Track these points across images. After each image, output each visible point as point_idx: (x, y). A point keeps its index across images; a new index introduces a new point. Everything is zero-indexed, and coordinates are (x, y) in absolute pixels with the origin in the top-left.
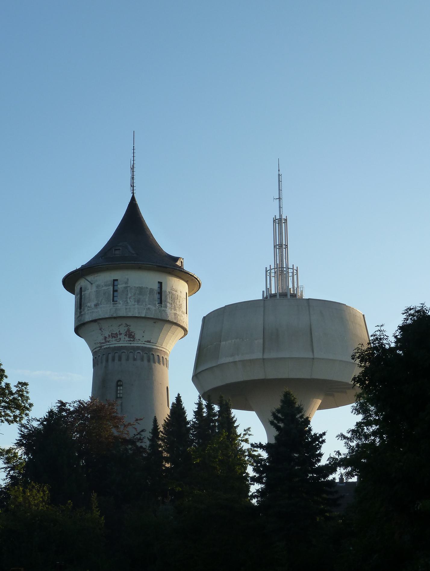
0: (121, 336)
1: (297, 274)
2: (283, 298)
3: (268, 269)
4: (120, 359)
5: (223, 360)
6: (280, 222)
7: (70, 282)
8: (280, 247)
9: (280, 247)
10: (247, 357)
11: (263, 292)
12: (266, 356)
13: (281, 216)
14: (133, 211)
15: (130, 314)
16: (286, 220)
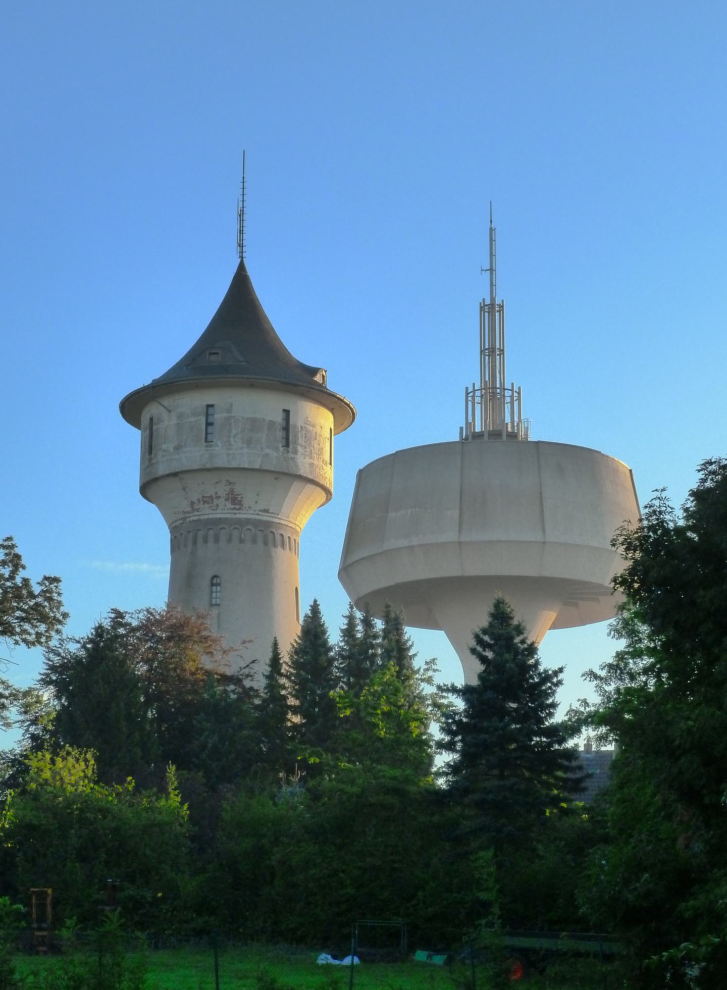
1: (519, 399)
3: (470, 389)
5: (392, 543)
7: (133, 407)
11: (461, 428)
14: (241, 283)
15: (234, 465)
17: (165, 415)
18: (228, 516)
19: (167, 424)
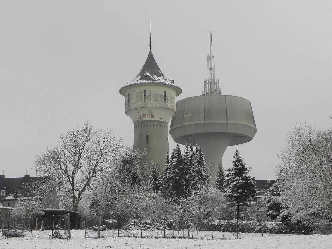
0: (148, 116)
1: (219, 83)
3: (205, 80)
4: (147, 126)
5: (185, 124)
7: (122, 91)
8: (211, 69)
9: (211, 69)
10: (197, 122)
11: (203, 91)
12: (206, 122)
13: (211, 54)
14: (150, 56)
15: (152, 106)
17: (133, 93)
18: (150, 120)
19: (133, 96)
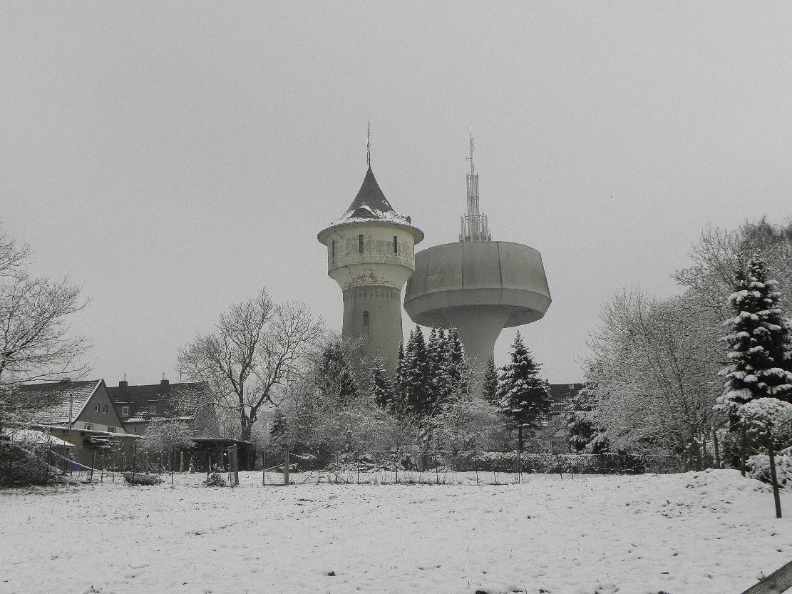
2: (476, 237)
6: (473, 179)
7: (323, 237)
8: (473, 199)
9: (473, 199)
12: (465, 287)
14: (370, 177)
15: (373, 261)
16: (477, 176)
17: (340, 240)
